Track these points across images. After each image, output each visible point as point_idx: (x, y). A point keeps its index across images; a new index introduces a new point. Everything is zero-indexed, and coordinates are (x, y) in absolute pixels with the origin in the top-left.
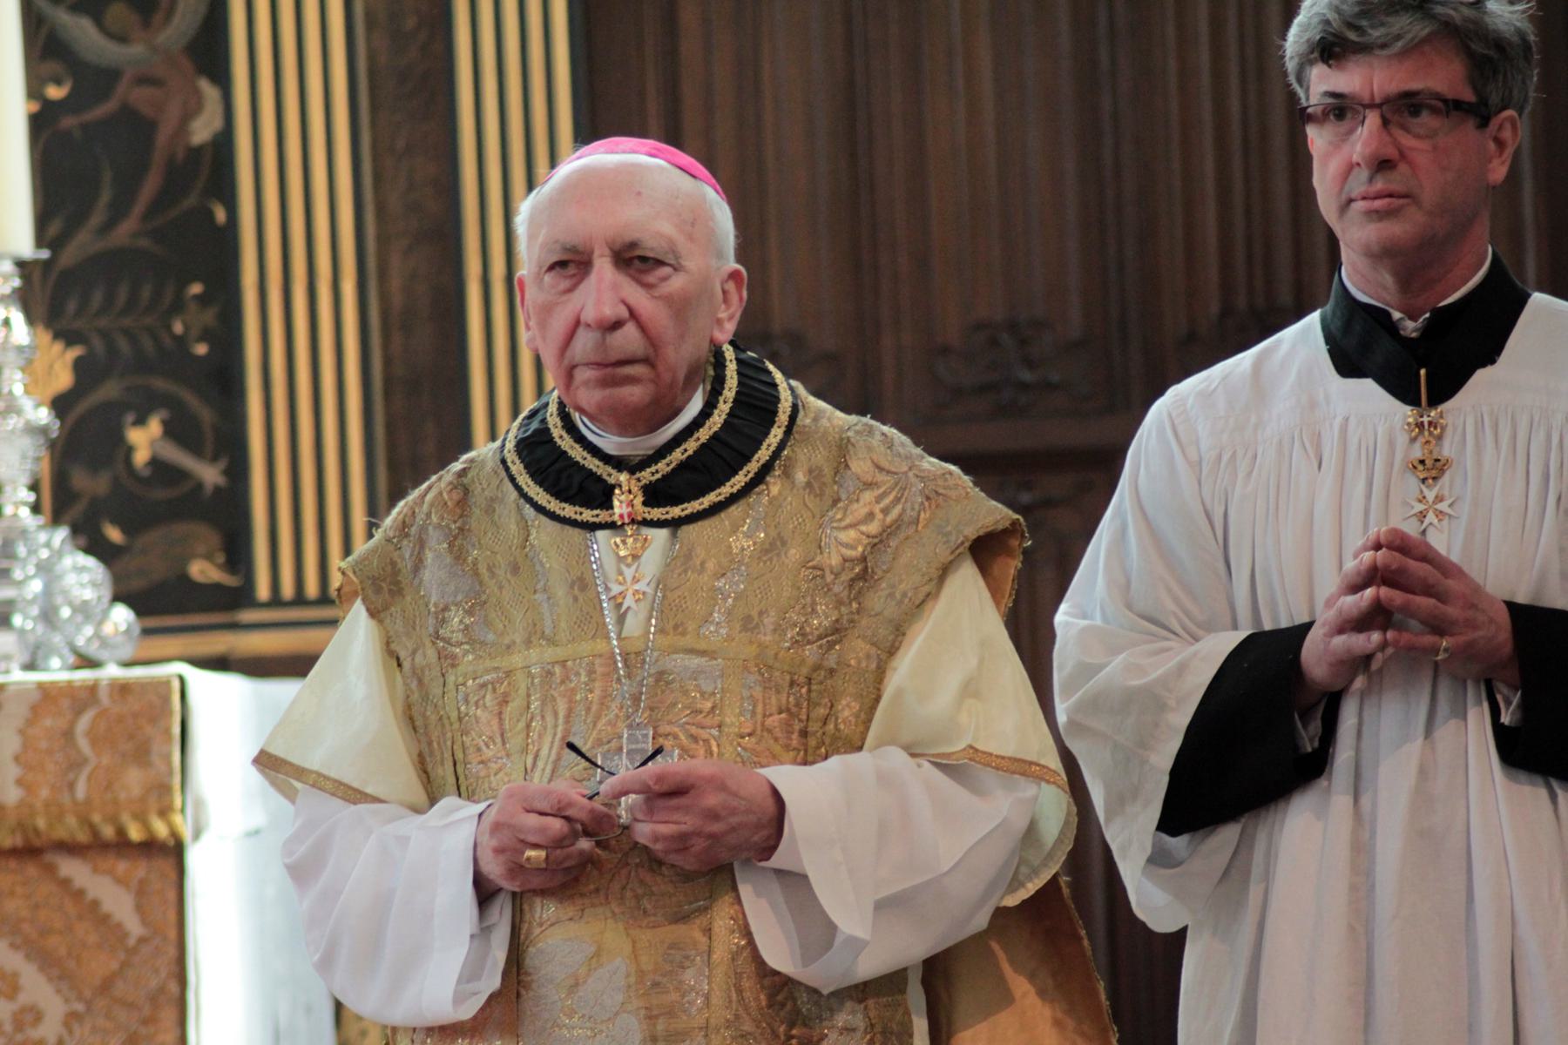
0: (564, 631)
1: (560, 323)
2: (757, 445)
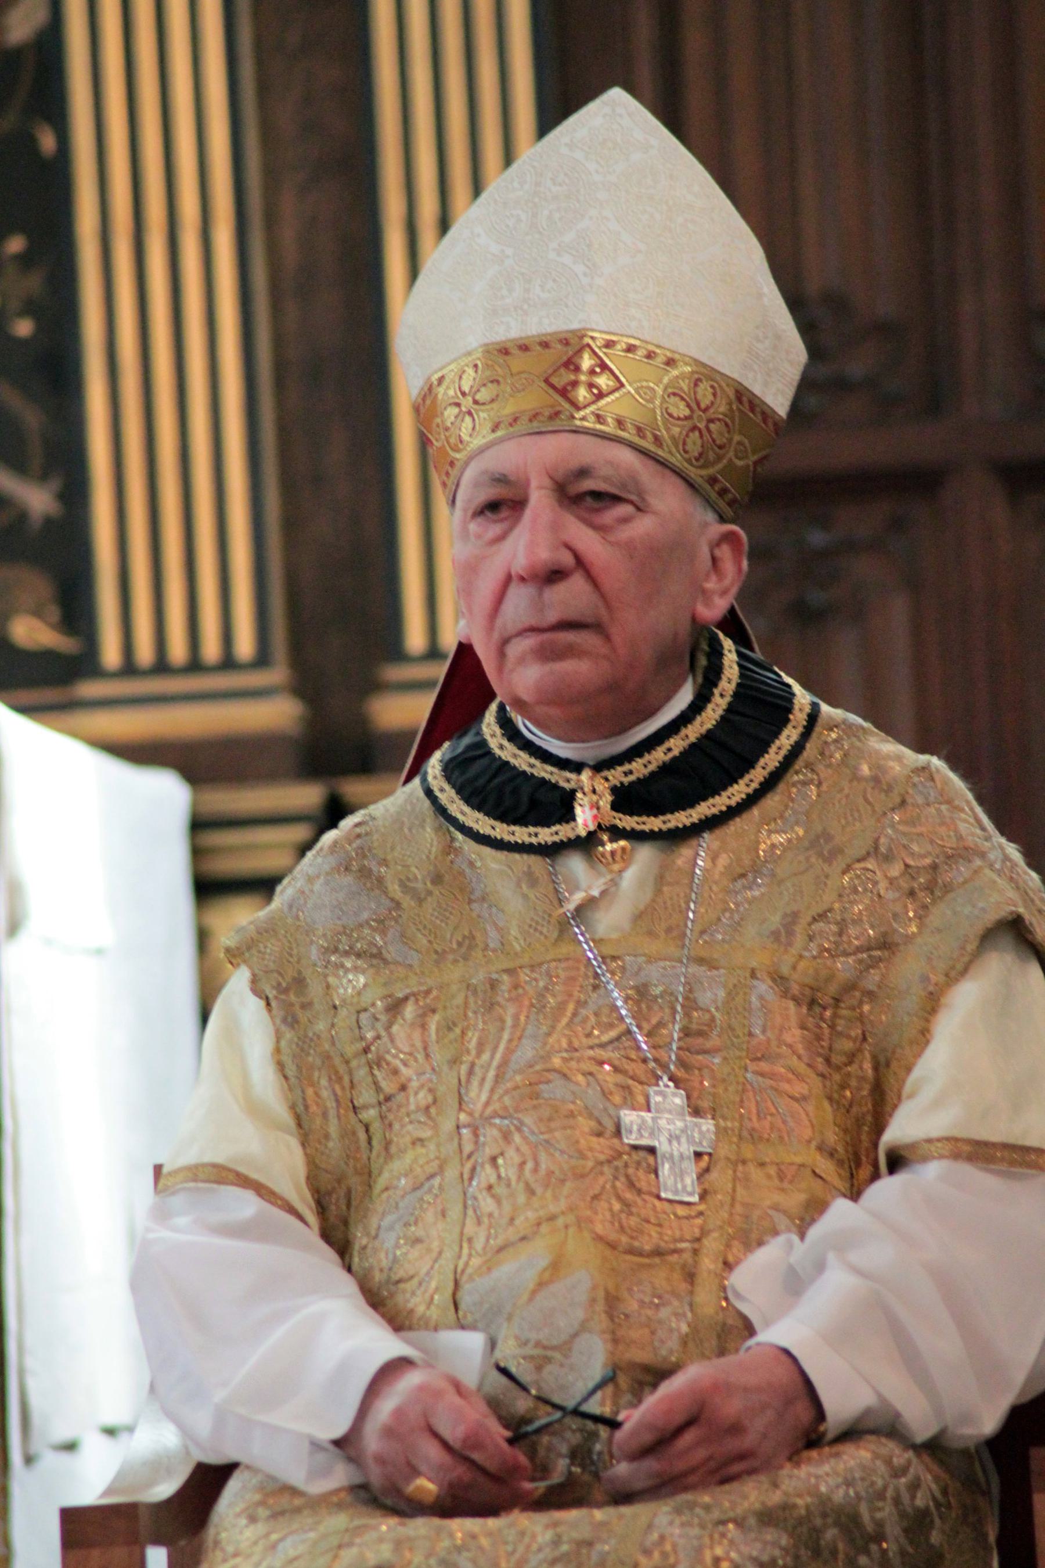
1: (486, 585)
2: (763, 748)
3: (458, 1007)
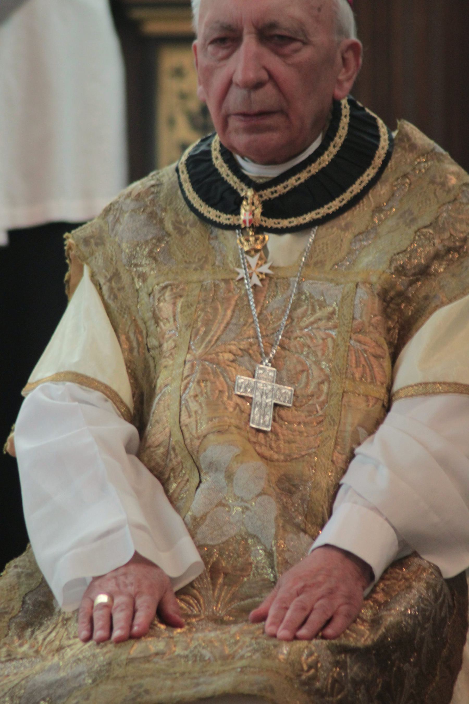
0: (231, 262)
3: (195, 296)
